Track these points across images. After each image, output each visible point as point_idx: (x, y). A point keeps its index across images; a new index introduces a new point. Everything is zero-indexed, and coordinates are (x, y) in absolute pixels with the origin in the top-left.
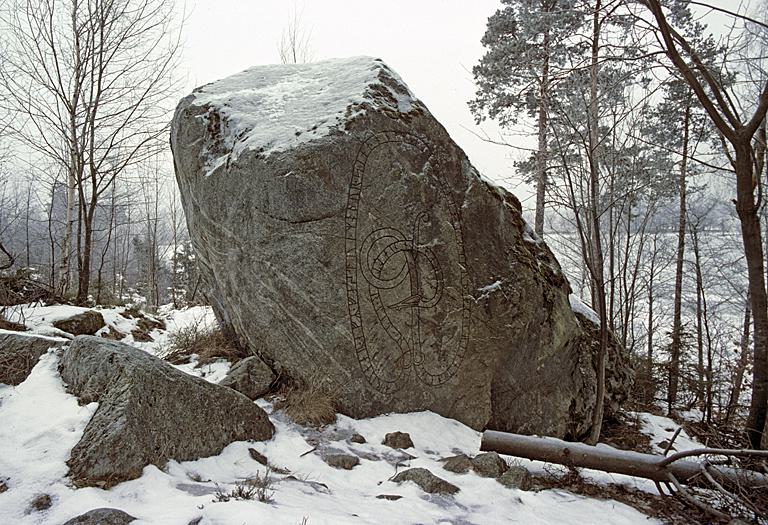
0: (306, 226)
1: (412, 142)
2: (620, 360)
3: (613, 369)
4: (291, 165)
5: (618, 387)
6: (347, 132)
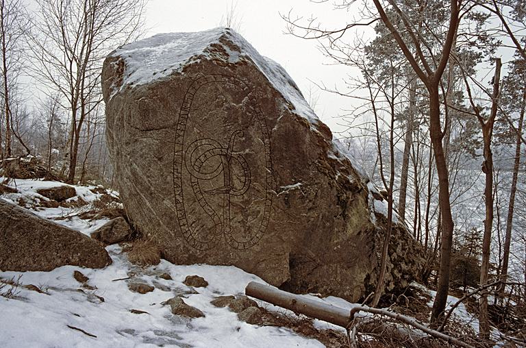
1: (235, 82)
2: (412, 251)
3: (405, 256)
5: (407, 269)
6: (183, 73)
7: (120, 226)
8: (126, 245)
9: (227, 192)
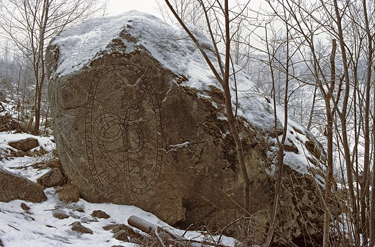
6: (90, 67)
7: (56, 175)
8: (59, 188)
9: (126, 151)
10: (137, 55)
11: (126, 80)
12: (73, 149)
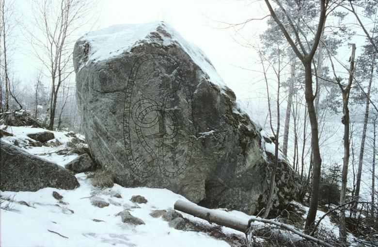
0: (106, 95)
1: (167, 59)
3: (287, 183)
4: (103, 67)
6: (130, 53)
7: (86, 160)
8: (90, 173)
10: (174, 48)
11: (164, 70)
12: (109, 134)
